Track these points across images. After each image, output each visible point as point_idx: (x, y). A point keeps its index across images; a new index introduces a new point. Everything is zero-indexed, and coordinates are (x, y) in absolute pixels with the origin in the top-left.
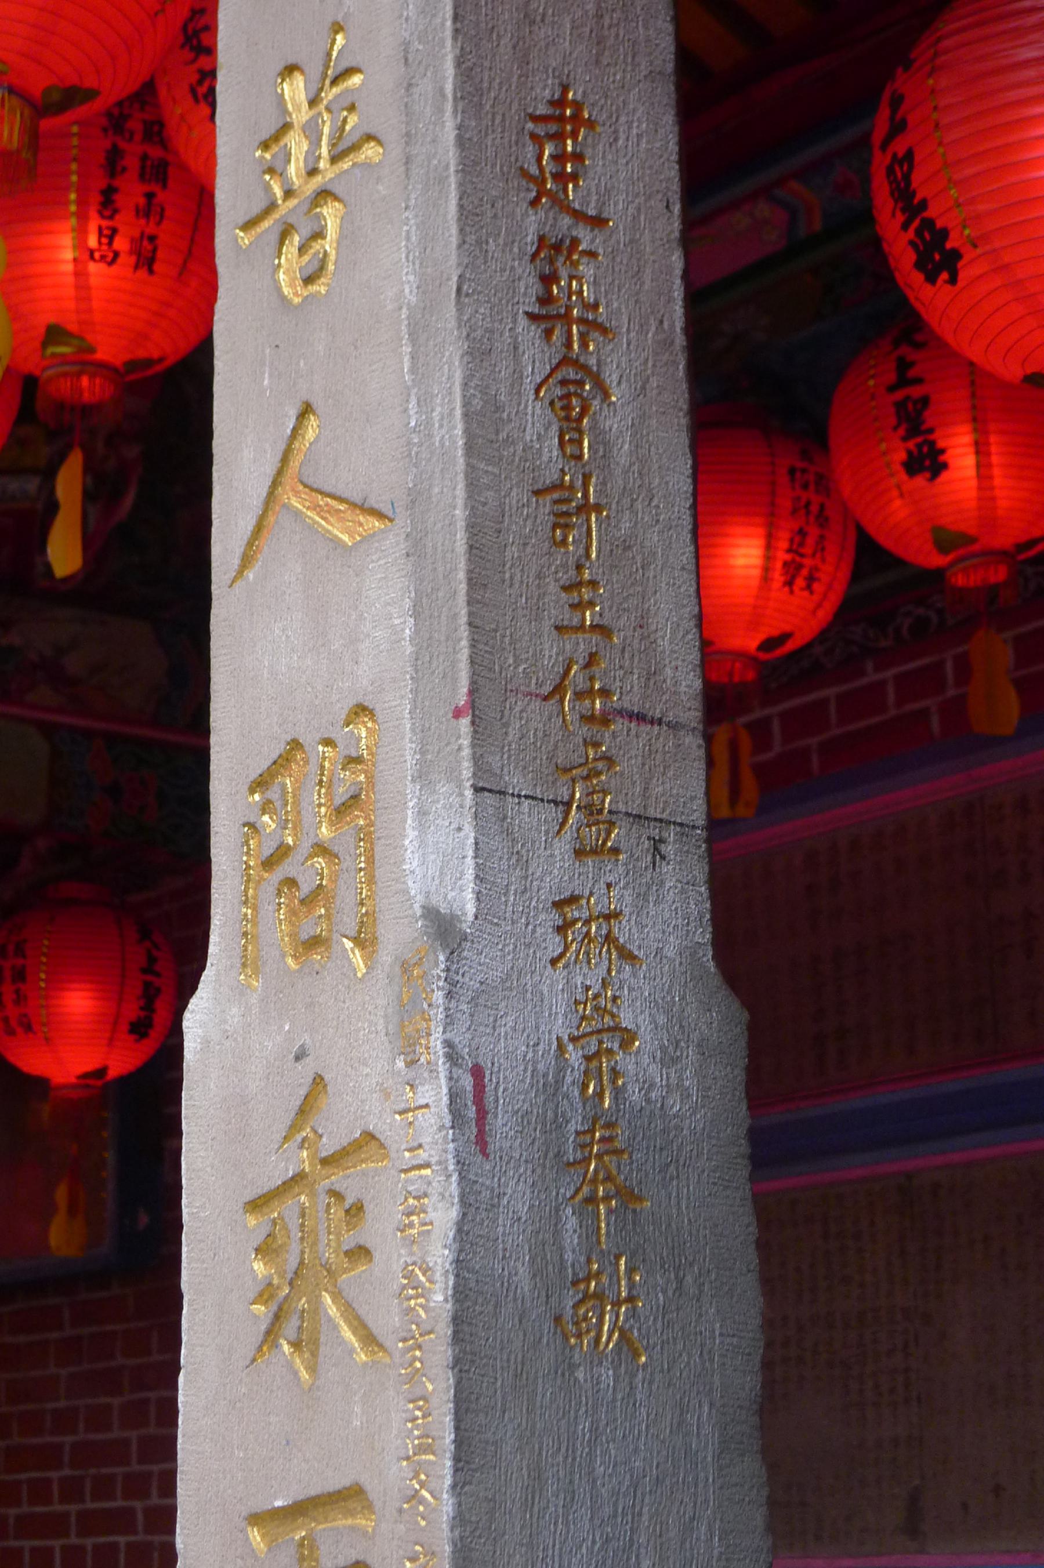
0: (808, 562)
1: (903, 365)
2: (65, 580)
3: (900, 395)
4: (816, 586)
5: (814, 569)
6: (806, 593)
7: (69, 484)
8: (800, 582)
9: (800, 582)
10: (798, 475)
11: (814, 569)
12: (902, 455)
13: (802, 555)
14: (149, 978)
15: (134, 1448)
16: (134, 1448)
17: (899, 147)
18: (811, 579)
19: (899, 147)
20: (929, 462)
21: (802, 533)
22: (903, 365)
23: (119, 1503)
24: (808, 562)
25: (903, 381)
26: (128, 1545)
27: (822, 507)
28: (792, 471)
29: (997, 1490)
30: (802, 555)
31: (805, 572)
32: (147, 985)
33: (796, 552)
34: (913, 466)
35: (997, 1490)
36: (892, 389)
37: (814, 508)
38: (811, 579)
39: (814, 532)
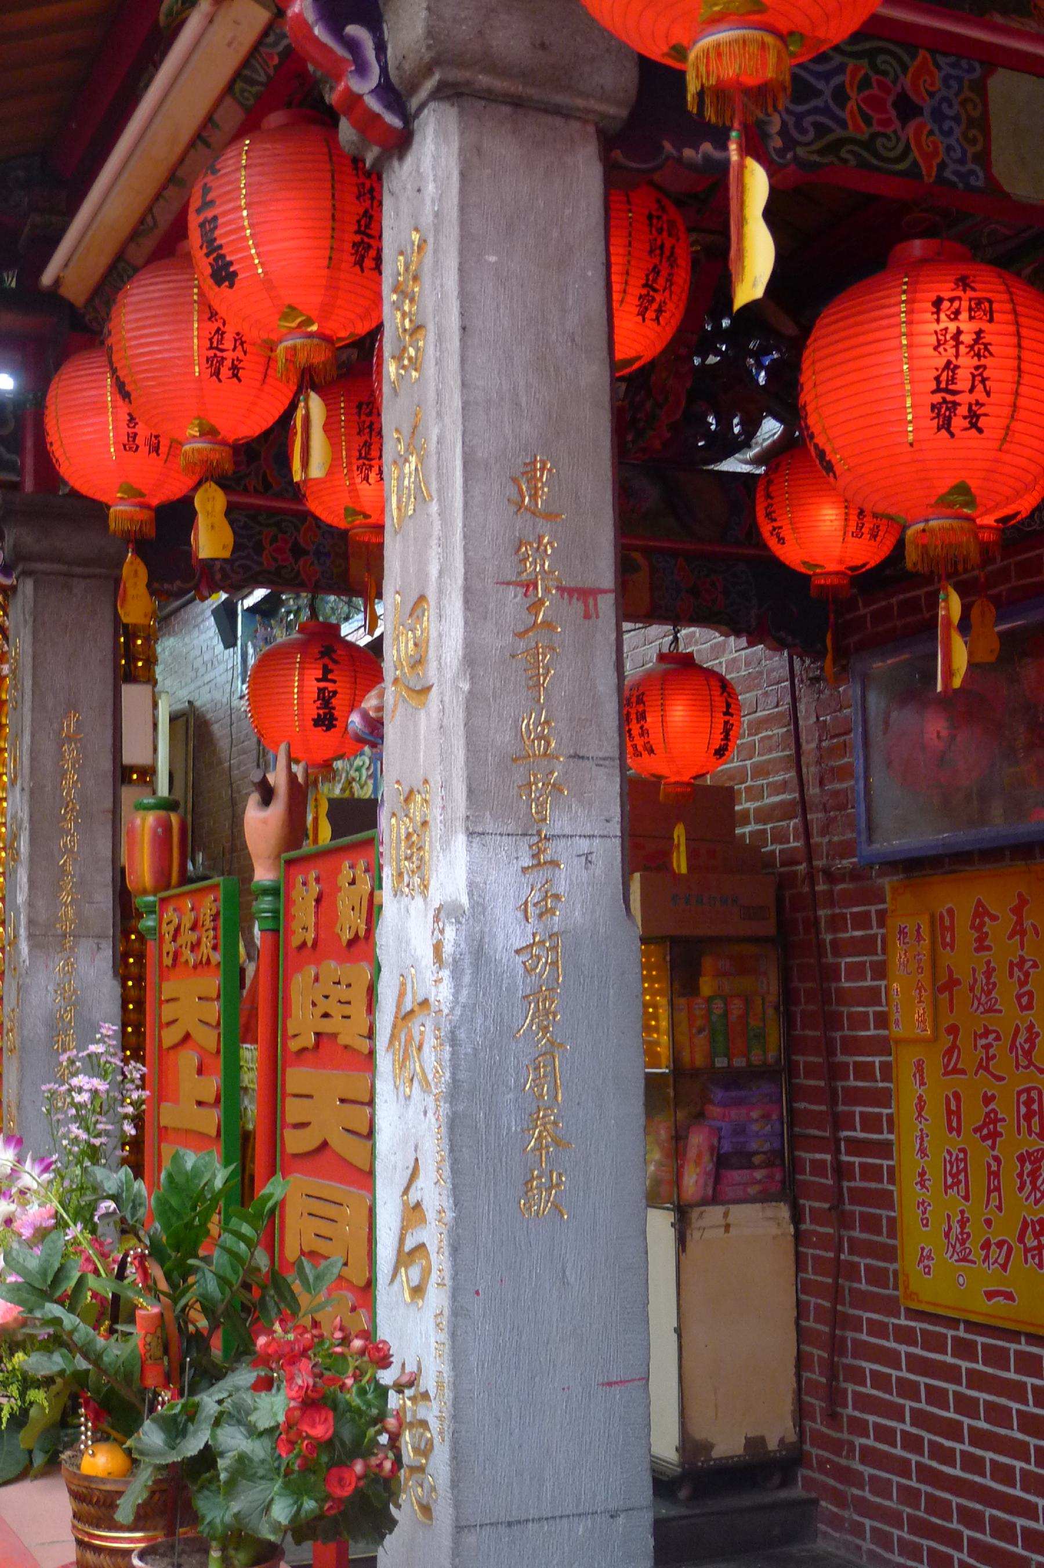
0: (658, 297)
3: (322, 684)
4: (982, 422)
5: (663, 303)
6: (655, 324)
7: (679, 833)
8: (958, 422)
9: (650, 314)
11: (663, 303)
14: (727, 718)
15: (1013, 574)
16: (1013, 574)
17: (209, 214)
18: (659, 311)
19: (209, 214)
21: (656, 270)
23: (869, 983)
24: (658, 297)
25: (324, 679)
27: (673, 248)
28: (650, 217)
31: (655, 306)
32: (726, 723)
37: (967, 338)
38: (659, 311)
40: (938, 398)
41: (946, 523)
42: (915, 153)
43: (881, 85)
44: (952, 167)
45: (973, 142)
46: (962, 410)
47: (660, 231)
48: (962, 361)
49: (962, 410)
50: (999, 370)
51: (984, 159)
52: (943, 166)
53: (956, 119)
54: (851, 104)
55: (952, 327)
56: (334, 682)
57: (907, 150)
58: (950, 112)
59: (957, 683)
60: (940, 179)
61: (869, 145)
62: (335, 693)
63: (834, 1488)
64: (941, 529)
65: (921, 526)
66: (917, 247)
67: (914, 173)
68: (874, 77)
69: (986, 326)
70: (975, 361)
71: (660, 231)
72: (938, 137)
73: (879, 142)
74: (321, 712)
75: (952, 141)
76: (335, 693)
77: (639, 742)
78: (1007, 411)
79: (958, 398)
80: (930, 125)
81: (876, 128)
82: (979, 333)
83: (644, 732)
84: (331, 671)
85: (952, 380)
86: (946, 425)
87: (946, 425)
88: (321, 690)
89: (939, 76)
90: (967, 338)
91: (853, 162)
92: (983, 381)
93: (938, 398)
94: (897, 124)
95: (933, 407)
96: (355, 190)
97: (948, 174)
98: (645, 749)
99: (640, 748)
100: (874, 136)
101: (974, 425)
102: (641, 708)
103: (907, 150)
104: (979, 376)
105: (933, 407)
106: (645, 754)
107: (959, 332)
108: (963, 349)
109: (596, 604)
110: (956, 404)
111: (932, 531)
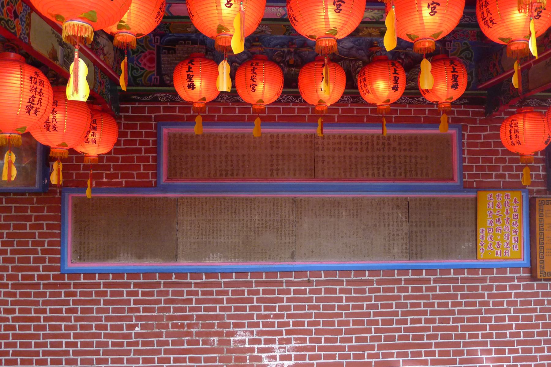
1: (190, 68)
2: (390, 52)
4: (38, 113)
8: (32, 112)
10: (33, 79)
12: (393, 86)
13: (33, 104)
20: (192, 86)
22: (190, 68)
25: (189, 71)
26: (535, 316)
28: (31, 78)
29: (312, 252)
30: (33, 104)
33: (31, 103)
34: (189, 87)
35: (312, 252)
36: (187, 72)
37: (38, 90)
39: (38, 97)
40: (29, 104)
41: (16, 135)
42: (16, 28)
43: (12, 6)
44: (23, 35)
45: (27, 30)
46: (34, 109)
47: (36, 83)
48: (37, 96)
49: (34, 109)
51: (28, 35)
52: (21, 34)
53: (25, 22)
54: (5, 9)
56: (192, 72)
57: (15, 27)
58: (24, 20)
59: (13, 179)
60: (20, 38)
61: (7, 22)
64: (15, 137)
65: (9, 135)
66: (12, 55)
67: (15, 34)
68: (10, 3)
69: (43, 88)
70: (39, 97)
71: (36, 83)
72: (21, 26)
73: (10, 22)
75: (23, 28)
76: (193, 76)
77: (515, 141)
78: (43, 111)
79: (34, 106)
80: (20, 22)
81: (9, 18)
85: (33, 100)
86: (29, 112)
87: (29, 112)
88: (453, 75)
89: (23, 8)
90: (38, 90)
91: (3, 26)
92: (41, 102)
93: (29, 104)
94: (13, 19)
95: (27, 106)
96: (30, 88)
97: (21, 37)
100: (9, 20)
101: (35, 113)
103: (15, 27)
104: (40, 101)
105: (27, 106)
107: (36, 88)
108: (37, 93)
109: (59, 178)
110: (33, 107)
111: (12, 137)
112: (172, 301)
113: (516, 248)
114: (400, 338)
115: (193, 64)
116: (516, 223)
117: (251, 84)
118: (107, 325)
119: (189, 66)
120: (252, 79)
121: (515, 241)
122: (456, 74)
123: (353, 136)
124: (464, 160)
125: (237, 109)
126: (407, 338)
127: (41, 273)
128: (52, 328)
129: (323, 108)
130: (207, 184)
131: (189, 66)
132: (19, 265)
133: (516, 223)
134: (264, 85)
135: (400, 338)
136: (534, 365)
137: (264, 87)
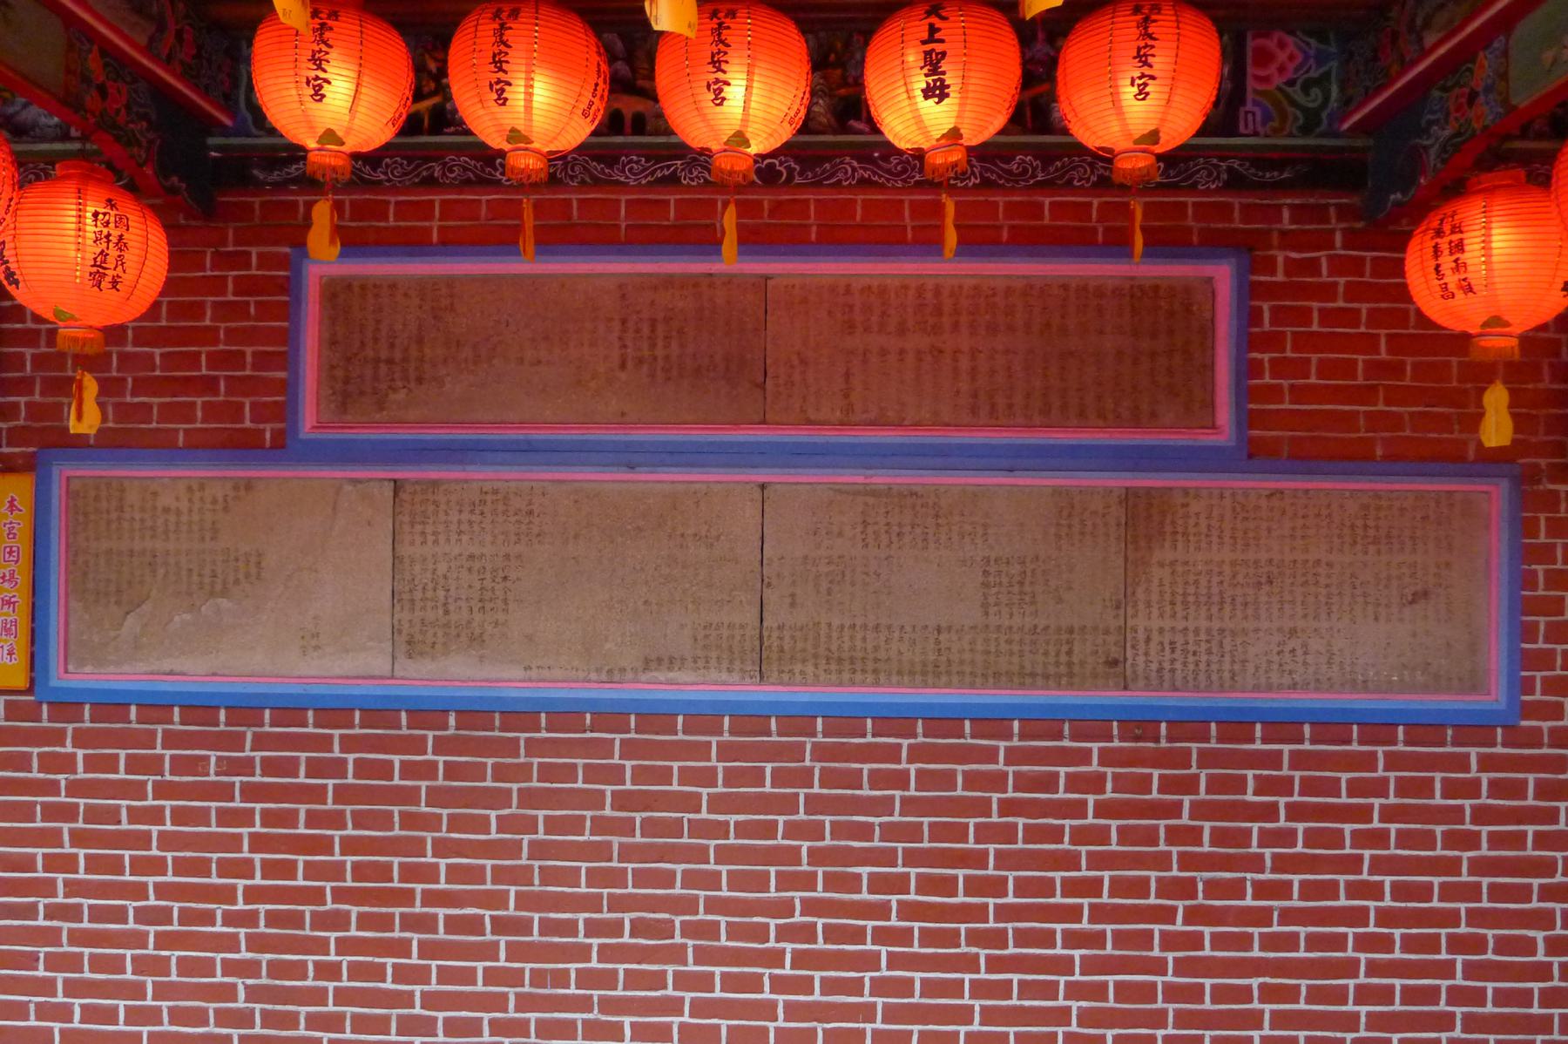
1: (933, 30)
25: (931, 40)
36: (924, 43)
37: (114, 239)
50: (131, 257)
55: (105, 231)
56: (942, 41)
62: (944, 54)
63: (461, 906)
74: (930, 79)
76: (944, 54)
77: (1451, 279)
82: (121, 237)
83: (1459, 266)
84: (939, 30)
88: (927, 54)
90: (114, 239)
98: (1461, 287)
99: (1452, 287)
102: (1455, 237)
106: (1460, 295)
107: (109, 235)
112: (1435, 866)
113: (10, 653)
114: (1269, 942)
115: (944, 19)
116: (12, 573)
117: (712, 77)
118: (1165, 960)
119: (931, 26)
120: (713, 62)
121: (8, 631)
122: (939, 47)
123: (930, 284)
124: (1254, 369)
125: (1332, 210)
126: (1290, 942)
127: (1467, 803)
128: (1049, 990)
129: (525, 162)
130: (1397, 487)
131: (931, 26)
132: (825, 791)
133: (12, 573)
134: (750, 80)
135: (1269, 942)
136: (150, 1034)
137: (748, 88)
